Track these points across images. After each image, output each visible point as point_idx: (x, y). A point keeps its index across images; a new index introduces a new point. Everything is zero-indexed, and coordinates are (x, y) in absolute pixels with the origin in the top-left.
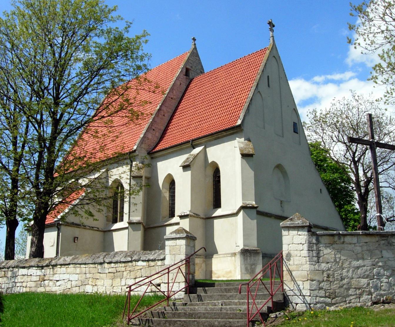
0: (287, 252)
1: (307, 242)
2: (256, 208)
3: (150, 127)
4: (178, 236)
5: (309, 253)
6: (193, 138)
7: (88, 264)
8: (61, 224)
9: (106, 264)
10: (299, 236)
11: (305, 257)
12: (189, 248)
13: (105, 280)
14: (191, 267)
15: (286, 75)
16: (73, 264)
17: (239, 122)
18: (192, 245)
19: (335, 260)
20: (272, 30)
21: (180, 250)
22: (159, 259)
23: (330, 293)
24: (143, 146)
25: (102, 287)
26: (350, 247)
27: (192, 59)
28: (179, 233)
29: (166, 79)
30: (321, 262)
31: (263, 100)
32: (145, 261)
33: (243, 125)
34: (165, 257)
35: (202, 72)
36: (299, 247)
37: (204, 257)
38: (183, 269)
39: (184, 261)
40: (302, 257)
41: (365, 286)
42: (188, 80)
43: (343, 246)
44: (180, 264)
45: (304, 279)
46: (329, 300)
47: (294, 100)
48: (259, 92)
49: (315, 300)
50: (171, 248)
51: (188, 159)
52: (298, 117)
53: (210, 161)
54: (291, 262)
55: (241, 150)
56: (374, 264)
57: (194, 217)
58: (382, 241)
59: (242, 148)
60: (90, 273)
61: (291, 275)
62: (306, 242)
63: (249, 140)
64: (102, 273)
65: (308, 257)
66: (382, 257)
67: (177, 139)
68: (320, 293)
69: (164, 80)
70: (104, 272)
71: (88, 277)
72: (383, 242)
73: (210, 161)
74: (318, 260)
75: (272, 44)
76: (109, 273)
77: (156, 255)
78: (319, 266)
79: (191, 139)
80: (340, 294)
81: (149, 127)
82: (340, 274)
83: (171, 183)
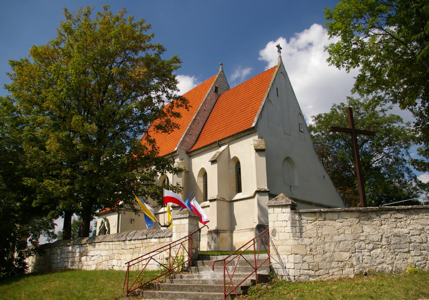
0: (272, 228)
1: (290, 219)
4: (182, 216)
6: (219, 139)
7: (114, 241)
11: (288, 233)
12: (193, 226)
14: (195, 242)
16: (103, 242)
17: (254, 125)
18: (195, 224)
19: (317, 235)
21: (184, 229)
22: (168, 236)
23: (313, 266)
24: (182, 147)
27: (220, 80)
28: (183, 214)
32: (157, 238)
33: (257, 127)
34: (172, 235)
35: (228, 89)
37: (230, 232)
39: (188, 237)
42: (217, 96)
44: (184, 240)
45: (288, 253)
46: (313, 272)
47: (299, 106)
49: (299, 273)
51: (215, 155)
53: (232, 157)
54: (276, 238)
55: (255, 147)
57: (221, 200)
59: (256, 144)
60: (116, 249)
63: (262, 138)
64: (124, 248)
67: (208, 141)
68: (304, 266)
70: (126, 248)
71: (115, 253)
73: (232, 157)
74: (301, 235)
75: (280, 62)
76: (130, 249)
78: (302, 241)
79: (218, 140)
80: (323, 266)
82: (323, 248)
83: (204, 174)
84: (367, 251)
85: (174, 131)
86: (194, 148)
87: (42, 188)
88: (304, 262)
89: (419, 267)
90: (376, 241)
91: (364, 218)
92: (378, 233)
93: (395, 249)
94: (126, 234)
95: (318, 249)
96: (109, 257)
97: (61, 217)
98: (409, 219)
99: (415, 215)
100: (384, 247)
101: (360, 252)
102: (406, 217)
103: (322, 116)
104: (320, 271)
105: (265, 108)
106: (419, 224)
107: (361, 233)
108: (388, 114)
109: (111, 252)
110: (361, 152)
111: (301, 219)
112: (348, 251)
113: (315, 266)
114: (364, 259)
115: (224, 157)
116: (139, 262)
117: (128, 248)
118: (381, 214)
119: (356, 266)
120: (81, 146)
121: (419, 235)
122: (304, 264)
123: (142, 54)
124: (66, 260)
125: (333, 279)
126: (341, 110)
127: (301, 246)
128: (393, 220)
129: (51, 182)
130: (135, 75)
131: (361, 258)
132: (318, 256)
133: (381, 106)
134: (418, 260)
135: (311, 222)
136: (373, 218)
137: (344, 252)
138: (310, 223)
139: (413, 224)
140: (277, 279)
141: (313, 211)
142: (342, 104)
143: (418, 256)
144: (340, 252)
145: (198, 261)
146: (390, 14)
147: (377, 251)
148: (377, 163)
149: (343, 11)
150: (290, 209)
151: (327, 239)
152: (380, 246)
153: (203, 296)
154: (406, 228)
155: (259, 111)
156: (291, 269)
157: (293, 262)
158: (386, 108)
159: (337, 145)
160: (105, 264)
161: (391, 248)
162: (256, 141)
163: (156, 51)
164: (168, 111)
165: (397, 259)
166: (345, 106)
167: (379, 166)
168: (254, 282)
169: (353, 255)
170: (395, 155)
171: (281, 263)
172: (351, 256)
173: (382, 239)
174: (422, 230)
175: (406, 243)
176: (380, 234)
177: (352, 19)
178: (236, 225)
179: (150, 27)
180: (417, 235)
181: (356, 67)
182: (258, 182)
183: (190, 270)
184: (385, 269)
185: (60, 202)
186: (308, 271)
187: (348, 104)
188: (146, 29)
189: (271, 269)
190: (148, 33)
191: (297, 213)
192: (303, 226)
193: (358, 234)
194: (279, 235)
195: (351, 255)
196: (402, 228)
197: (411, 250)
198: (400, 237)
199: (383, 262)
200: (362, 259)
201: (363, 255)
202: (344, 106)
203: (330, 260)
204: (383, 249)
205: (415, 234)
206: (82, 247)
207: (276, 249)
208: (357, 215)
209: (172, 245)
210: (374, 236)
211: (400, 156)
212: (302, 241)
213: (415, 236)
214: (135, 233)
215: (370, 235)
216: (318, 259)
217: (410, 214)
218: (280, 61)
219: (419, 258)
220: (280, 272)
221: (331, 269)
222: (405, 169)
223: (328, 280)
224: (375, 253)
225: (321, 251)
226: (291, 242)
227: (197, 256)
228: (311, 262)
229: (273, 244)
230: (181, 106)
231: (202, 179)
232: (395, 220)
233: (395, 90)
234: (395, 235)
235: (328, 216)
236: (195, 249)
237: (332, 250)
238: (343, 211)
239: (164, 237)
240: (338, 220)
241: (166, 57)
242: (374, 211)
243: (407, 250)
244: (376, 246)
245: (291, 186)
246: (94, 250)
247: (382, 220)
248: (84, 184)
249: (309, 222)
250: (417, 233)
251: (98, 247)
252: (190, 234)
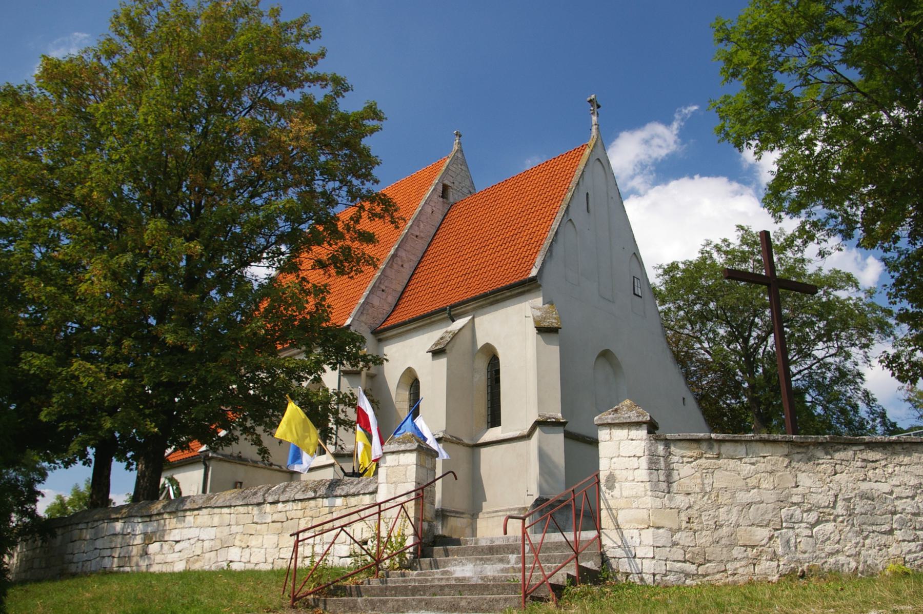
0: (607, 473)
1: (646, 453)
2: (564, 424)
3: (377, 285)
4: (403, 447)
6: (453, 303)
7: (235, 506)
8: (212, 458)
9: (268, 505)
11: (642, 482)
13: (265, 537)
16: (206, 508)
21: (405, 475)
24: (363, 318)
25: (259, 550)
27: (454, 169)
28: (404, 443)
30: (675, 492)
34: (377, 488)
36: (631, 463)
38: (411, 507)
41: (763, 542)
42: (446, 205)
45: (641, 524)
46: (694, 567)
47: (634, 239)
48: (570, 220)
51: (442, 338)
54: (616, 492)
55: (535, 321)
57: (452, 442)
59: (537, 316)
60: (237, 524)
61: (615, 519)
63: (551, 303)
64: (260, 522)
67: (423, 306)
70: (264, 521)
71: (235, 532)
73: (480, 344)
74: (669, 487)
76: (273, 522)
77: (361, 485)
78: (670, 500)
79: (449, 304)
80: (715, 556)
82: (714, 517)
83: (413, 384)
84: (806, 528)
85: (362, 272)
86: (390, 321)
87: (62, 380)
88: (675, 544)
89: (911, 564)
90: (824, 507)
91: (800, 456)
92: (829, 491)
93: (863, 524)
94: (264, 489)
95: (703, 518)
96: (220, 541)
97: (81, 462)
98: (891, 463)
99: (904, 457)
100: (841, 519)
101: (790, 528)
102: (886, 459)
103: (678, 267)
104: (707, 565)
105: (560, 238)
106: (911, 475)
107: (794, 487)
108: (827, 266)
109: (226, 530)
110: (763, 353)
111: (670, 454)
112: (766, 526)
113: (697, 554)
114: (800, 542)
115: (464, 341)
116: (314, 536)
117: (269, 520)
118: (834, 451)
119: (782, 556)
120: (162, 288)
121: (911, 497)
122: (674, 549)
123: (295, 96)
124: (108, 552)
125: (735, 583)
126: (723, 256)
127: (668, 510)
128: (859, 464)
129: (88, 365)
130: (289, 137)
131: (793, 541)
132: (704, 533)
133: (818, 243)
134: (910, 550)
135: (690, 460)
136: (819, 458)
137: (758, 526)
138: (687, 462)
139: (899, 475)
140: (617, 580)
141: (694, 438)
142: (725, 240)
143: (909, 542)
144: (750, 526)
145: (436, 548)
146: (851, 41)
147: (826, 527)
148: (798, 380)
149: (756, 27)
150: (646, 431)
151: (724, 498)
152: (832, 517)
153: (469, 603)
154: (886, 482)
155: (547, 243)
156: (648, 560)
158: (829, 249)
159: (711, 335)
160: (210, 559)
161: (855, 522)
162: (539, 309)
163: (329, 90)
164: (348, 228)
165: (866, 546)
166: (732, 246)
167: (803, 385)
168: (572, 580)
169: (776, 533)
170: (840, 362)
171: (625, 546)
172: (773, 535)
173: (835, 502)
174: (918, 488)
175: (886, 514)
176: (832, 492)
177: (772, 45)
178: (486, 501)
179: (318, 35)
180: (907, 497)
181: (776, 148)
182: (541, 402)
183: (418, 566)
184: (843, 565)
185: (102, 417)
187: (738, 242)
188: (309, 39)
189: (604, 560)
190: (311, 48)
191: (662, 440)
192: (673, 469)
193: (787, 491)
194: (621, 486)
195: (772, 533)
196: (876, 481)
197: (896, 529)
198: (873, 500)
199: (838, 552)
200: (796, 542)
201: (797, 535)
202: (728, 246)
203: (728, 543)
204: (838, 524)
205: (904, 495)
206: (150, 521)
207: (614, 516)
208: (785, 449)
209: (301, 537)
210: (820, 496)
211: (849, 365)
212: (670, 500)
213: (904, 500)
214: (286, 487)
215: (812, 492)
216: (704, 539)
217: (895, 453)
219: (913, 546)
220: (624, 566)
221: (732, 561)
222: (860, 395)
223: (726, 585)
224: (821, 532)
225: (710, 523)
226: (649, 501)
227: (430, 538)
228: (689, 546)
229: (609, 506)
230: (381, 217)
231: (408, 393)
232: (864, 464)
233: (849, 209)
234: (864, 496)
235: (726, 449)
236: (427, 521)
237: (734, 522)
238: (756, 441)
239: (358, 494)
240: (747, 460)
241: (349, 105)
242: (821, 444)
243: (886, 527)
244: (824, 517)
246: (183, 528)
247: (836, 464)
248: (162, 376)
249: (685, 460)
250: (908, 494)
251: (192, 521)
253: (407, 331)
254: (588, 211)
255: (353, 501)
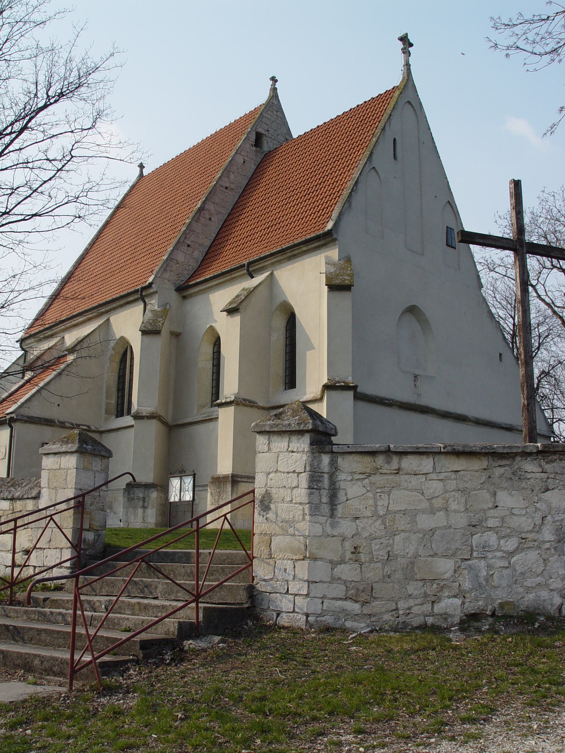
0: (263, 491)
1: (308, 468)
4: (64, 449)
5: (311, 494)
10: (291, 454)
11: (300, 504)
15: (433, 138)
17: (330, 226)
20: (407, 52)
24: (167, 275)
26: (414, 481)
27: (269, 116)
28: (67, 443)
29: (221, 154)
30: (339, 516)
31: (381, 182)
34: (39, 493)
40: (296, 503)
43: (397, 478)
44: (63, 506)
47: (449, 186)
48: (374, 168)
50: (51, 474)
51: (237, 296)
52: (456, 218)
55: (327, 278)
56: (473, 523)
58: (498, 468)
59: (331, 273)
62: (305, 467)
65: (308, 503)
66: (497, 506)
69: (219, 156)
72: (502, 470)
75: (406, 78)
81: (178, 242)
82: (387, 546)
88: (334, 580)
90: (527, 532)
144: (431, 556)
155: (346, 193)
157: (306, 578)
186: (345, 602)
195: (459, 564)
209: (19, 523)
218: (405, 75)
226: (304, 526)
245: (416, 377)
252: (81, 493)
253: (209, 288)
254: (395, 157)
255: (19, 505)
